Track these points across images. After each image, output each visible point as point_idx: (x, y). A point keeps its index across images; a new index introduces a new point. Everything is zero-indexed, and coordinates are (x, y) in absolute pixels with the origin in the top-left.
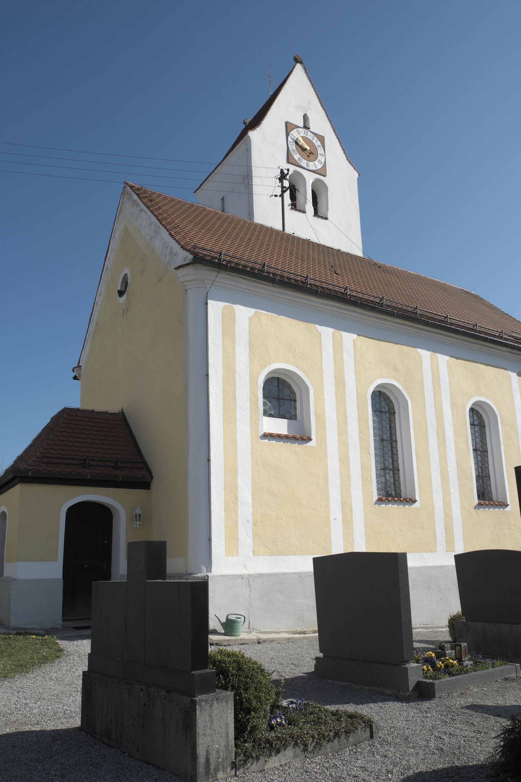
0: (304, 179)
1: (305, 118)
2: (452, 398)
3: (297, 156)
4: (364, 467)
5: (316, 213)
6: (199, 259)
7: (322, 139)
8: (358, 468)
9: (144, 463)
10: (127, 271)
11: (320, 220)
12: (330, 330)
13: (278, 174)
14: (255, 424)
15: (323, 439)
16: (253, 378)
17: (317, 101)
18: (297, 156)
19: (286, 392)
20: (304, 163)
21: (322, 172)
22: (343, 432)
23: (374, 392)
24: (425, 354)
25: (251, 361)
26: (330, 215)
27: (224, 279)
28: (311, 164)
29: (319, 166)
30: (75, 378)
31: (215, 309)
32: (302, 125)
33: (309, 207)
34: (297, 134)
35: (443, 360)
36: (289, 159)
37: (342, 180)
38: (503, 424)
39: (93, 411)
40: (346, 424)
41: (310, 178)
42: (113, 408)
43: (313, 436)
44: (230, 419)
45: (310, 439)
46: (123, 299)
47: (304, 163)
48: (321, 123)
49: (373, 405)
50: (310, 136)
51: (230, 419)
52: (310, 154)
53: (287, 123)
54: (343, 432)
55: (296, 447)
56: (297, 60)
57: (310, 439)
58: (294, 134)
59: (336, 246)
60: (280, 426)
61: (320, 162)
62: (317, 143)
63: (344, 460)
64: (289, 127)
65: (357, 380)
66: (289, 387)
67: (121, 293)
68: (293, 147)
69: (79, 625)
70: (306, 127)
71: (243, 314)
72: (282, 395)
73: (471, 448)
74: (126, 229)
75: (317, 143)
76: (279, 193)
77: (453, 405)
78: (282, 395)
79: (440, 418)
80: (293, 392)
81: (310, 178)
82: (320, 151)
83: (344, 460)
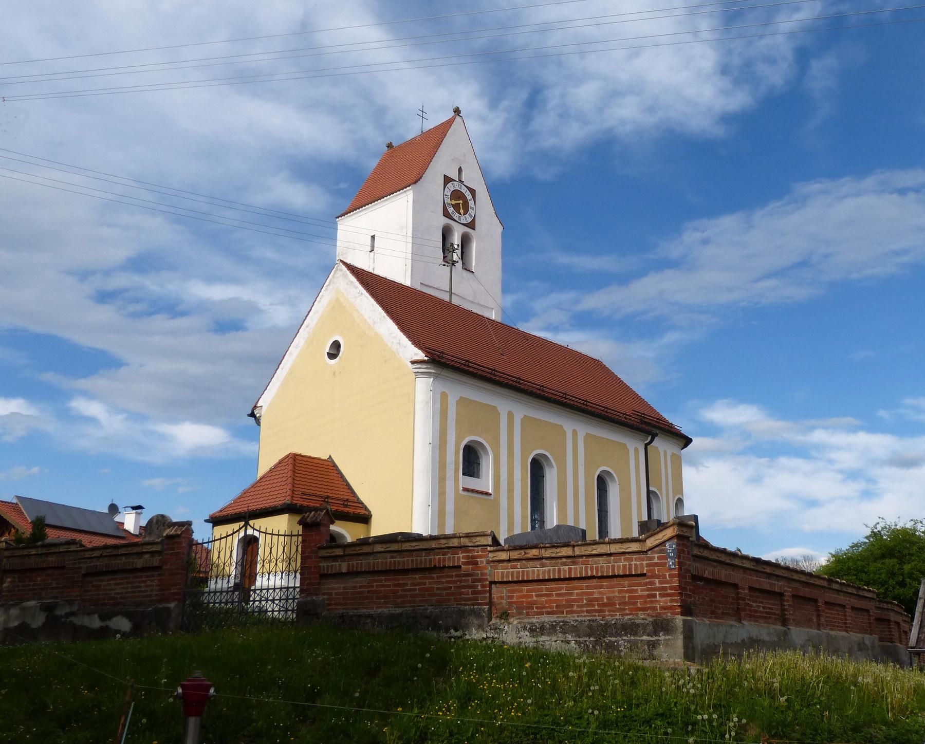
14: (456, 480)
20: (456, 216)
21: (472, 225)
47: (456, 216)
61: (470, 215)
64: (447, 180)
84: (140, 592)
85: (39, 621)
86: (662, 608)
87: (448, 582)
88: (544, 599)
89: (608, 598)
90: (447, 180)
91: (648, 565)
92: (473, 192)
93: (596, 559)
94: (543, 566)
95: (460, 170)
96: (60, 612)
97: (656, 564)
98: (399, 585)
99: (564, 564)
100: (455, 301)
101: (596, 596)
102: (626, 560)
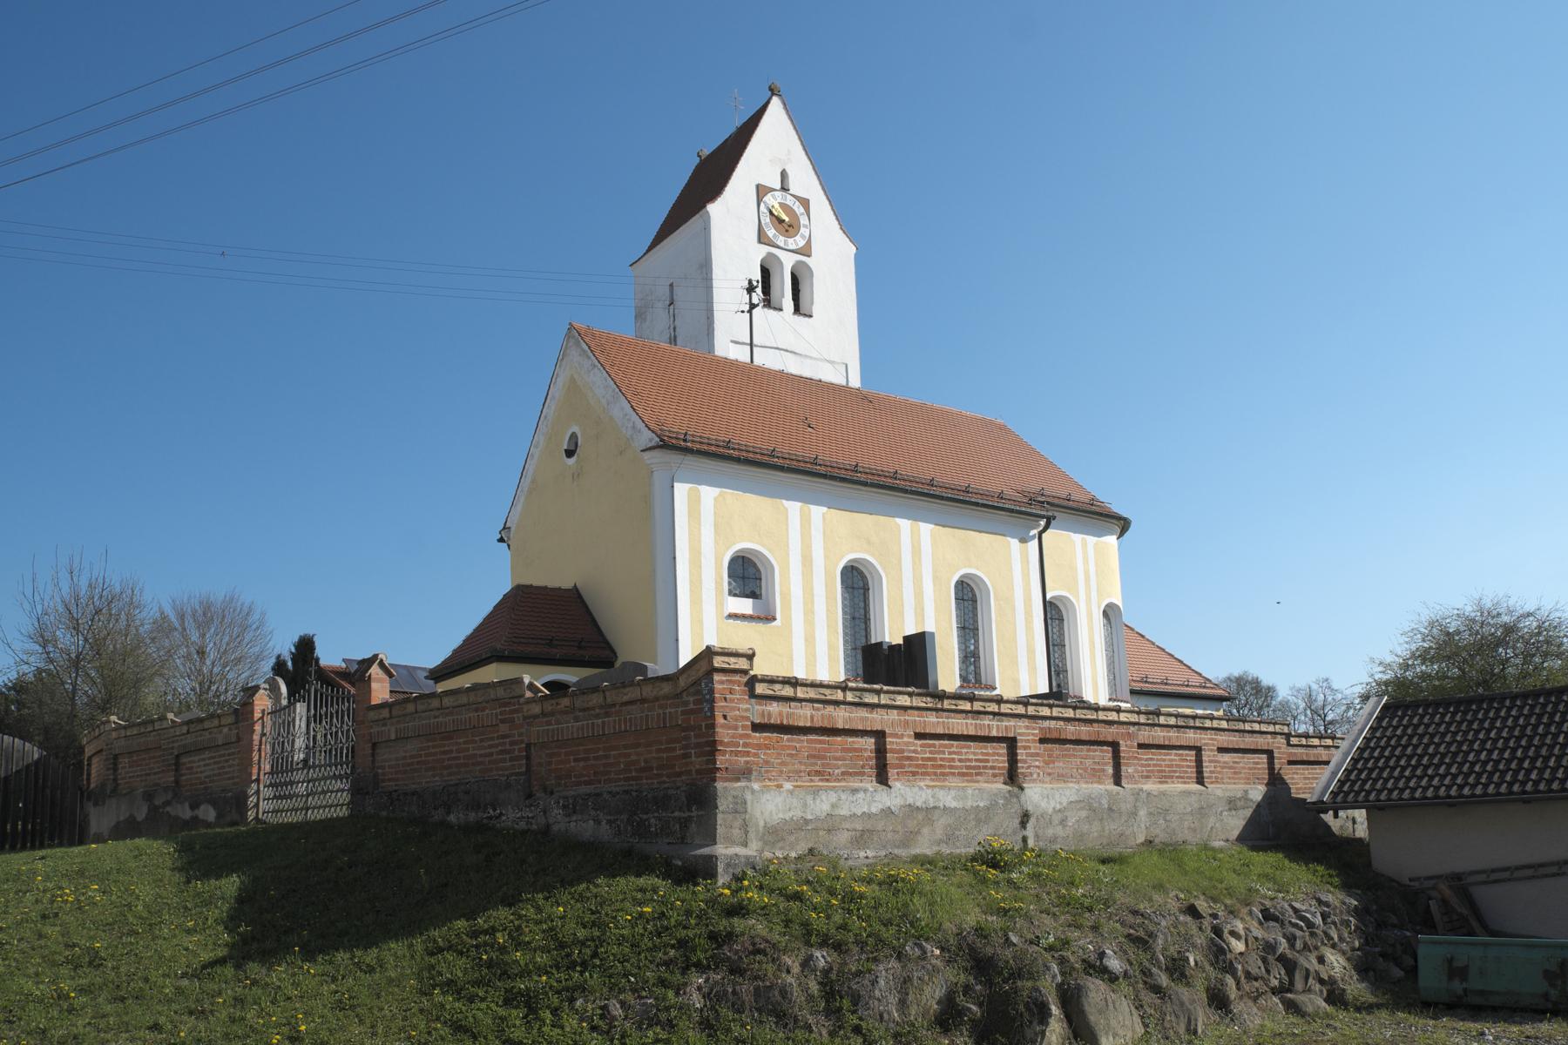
0: (781, 263)
1: (784, 175)
2: (935, 571)
3: (771, 232)
4: (831, 647)
5: (797, 310)
6: (667, 444)
7: (805, 203)
8: (825, 648)
9: (607, 643)
10: (575, 429)
11: (801, 318)
12: (798, 505)
13: (746, 284)
14: (720, 604)
15: (788, 618)
16: (718, 559)
17: (800, 148)
18: (771, 232)
19: (751, 570)
20: (781, 241)
21: (806, 251)
22: (809, 612)
23: (845, 568)
24: (904, 524)
25: (716, 542)
26: (816, 310)
27: (690, 460)
28: (791, 241)
29: (802, 243)
30: (501, 540)
31: (681, 490)
32: (778, 186)
33: (788, 303)
34: (772, 200)
35: (926, 529)
36: (762, 238)
37: (832, 256)
38: (996, 599)
39: (531, 586)
40: (812, 602)
41: (788, 261)
42: (567, 584)
43: (778, 616)
44: (696, 601)
45: (774, 619)
46: (572, 461)
47: (781, 241)
48: (805, 181)
49: (843, 582)
50: (790, 201)
51: (696, 601)
52: (788, 226)
53: (758, 186)
54: (809, 612)
55: (760, 627)
56: (773, 91)
57: (774, 619)
58: (769, 199)
59: (816, 377)
60: (745, 606)
61: (803, 237)
62: (799, 209)
63: (810, 640)
64: (761, 191)
65: (826, 557)
66: (755, 565)
67: (570, 453)
68: (766, 219)
69: (732, 660)
70: (784, 189)
71: (708, 494)
72: (747, 575)
73: (955, 625)
74: (572, 380)
75: (799, 209)
76: (747, 308)
77: (936, 578)
78: (747, 575)
79: (919, 594)
80: (758, 571)
81: (788, 261)
82: (803, 220)
83: (810, 640)
84: (951, 767)
85: (141, 814)
86: (698, 772)
87: (491, 746)
88: (582, 764)
89: (646, 761)
90: (761, 191)
91: (683, 713)
92: (805, 203)
93: (630, 707)
94: (577, 719)
95: (784, 175)
96: (158, 802)
97: (692, 712)
98: (444, 753)
99: (597, 716)
100: (764, 359)
101: (634, 758)
102: (661, 707)
